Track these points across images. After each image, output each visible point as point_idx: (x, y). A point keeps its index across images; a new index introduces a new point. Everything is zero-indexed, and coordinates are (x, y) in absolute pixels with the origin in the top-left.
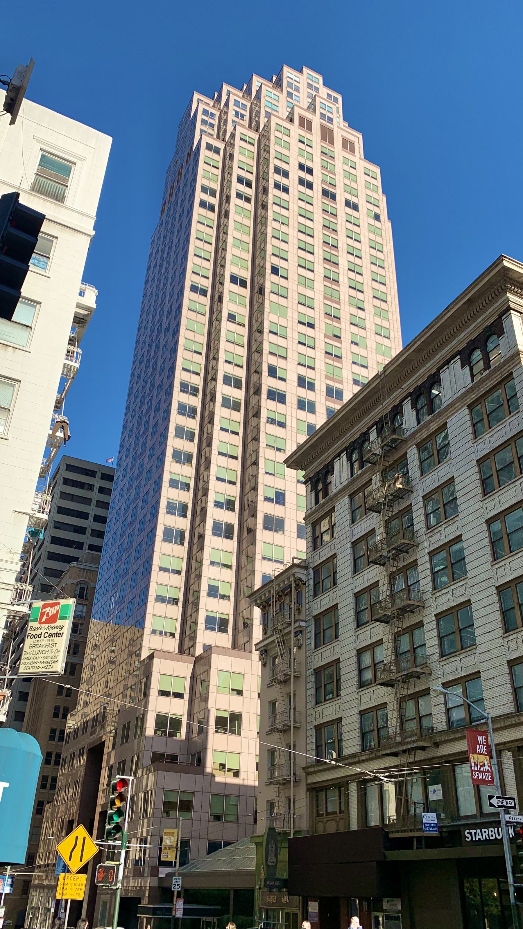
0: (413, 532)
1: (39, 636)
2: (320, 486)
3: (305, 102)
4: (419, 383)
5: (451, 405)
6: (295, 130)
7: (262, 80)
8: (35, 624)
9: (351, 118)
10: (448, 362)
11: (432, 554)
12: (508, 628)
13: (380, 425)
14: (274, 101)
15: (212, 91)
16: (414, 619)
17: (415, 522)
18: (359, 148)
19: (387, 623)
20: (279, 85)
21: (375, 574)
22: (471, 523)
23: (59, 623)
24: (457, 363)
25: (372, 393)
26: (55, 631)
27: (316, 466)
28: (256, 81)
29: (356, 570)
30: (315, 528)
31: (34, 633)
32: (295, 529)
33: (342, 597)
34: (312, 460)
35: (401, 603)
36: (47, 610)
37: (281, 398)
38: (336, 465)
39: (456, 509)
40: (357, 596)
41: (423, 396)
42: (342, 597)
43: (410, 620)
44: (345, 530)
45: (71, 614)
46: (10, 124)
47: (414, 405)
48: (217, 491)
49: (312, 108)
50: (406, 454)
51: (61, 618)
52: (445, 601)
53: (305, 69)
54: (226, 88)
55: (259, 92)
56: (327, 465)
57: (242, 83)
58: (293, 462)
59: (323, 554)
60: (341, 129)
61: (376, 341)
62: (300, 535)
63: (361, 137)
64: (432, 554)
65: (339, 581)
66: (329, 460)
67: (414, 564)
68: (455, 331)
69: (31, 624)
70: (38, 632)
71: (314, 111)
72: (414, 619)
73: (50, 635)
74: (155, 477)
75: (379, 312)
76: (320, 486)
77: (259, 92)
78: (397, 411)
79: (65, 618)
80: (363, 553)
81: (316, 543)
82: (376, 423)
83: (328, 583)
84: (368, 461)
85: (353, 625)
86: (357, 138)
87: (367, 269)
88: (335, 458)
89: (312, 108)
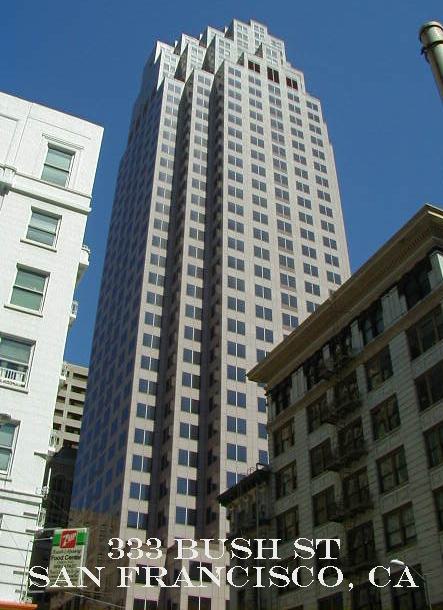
0: (363, 442)
1: (61, 558)
2: (280, 398)
3: (253, 48)
4: (365, 307)
5: (391, 330)
6: (245, 71)
7: (215, 31)
8: (57, 548)
9: (293, 59)
10: (387, 291)
11: (379, 462)
12: (432, 464)
13: (332, 344)
14: (228, 53)
15: (172, 39)
16: (354, 417)
17: (365, 433)
18: (301, 83)
19: (341, 522)
20: (230, 35)
21: (330, 479)
22: (410, 435)
23: (77, 548)
24: (394, 293)
25: (322, 316)
26: (74, 555)
27: (277, 378)
28: (211, 32)
29: (311, 430)
30: (278, 436)
31: (57, 555)
32: (256, 404)
33: (301, 499)
34: (273, 374)
35: (354, 505)
36: (67, 536)
37: (241, 307)
38: (295, 379)
39: (398, 423)
40: (315, 499)
41: (371, 317)
42: (301, 499)
43: (356, 467)
44: (306, 441)
45: (86, 540)
46: (18, 265)
47: (361, 328)
48: (187, 300)
49: (259, 52)
50: (355, 372)
51: (79, 544)
52: (378, 396)
53: (252, 23)
54: (184, 37)
55: (213, 41)
56: (286, 379)
57: (198, 32)
58: (258, 376)
59: (284, 460)
60: (285, 70)
61: (326, 265)
62: (261, 409)
63: (302, 75)
64: (379, 462)
65: (299, 485)
66: (288, 374)
67: (364, 470)
68: (397, 271)
69: (54, 548)
70: (60, 555)
71: (261, 56)
72: (354, 417)
73: (70, 558)
74: (134, 297)
75: (332, 260)
76: (280, 398)
77: (213, 41)
78: (346, 332)
79: (82, 544)
80: (321, 460)
81: (277, 448)
82: (328, 343)
83: (289, 488)
84: (323, 377)
85: (311, 525)
86: (299, 77)
87: (309, 146)
88: (293, 372)
89: (259, 52)
